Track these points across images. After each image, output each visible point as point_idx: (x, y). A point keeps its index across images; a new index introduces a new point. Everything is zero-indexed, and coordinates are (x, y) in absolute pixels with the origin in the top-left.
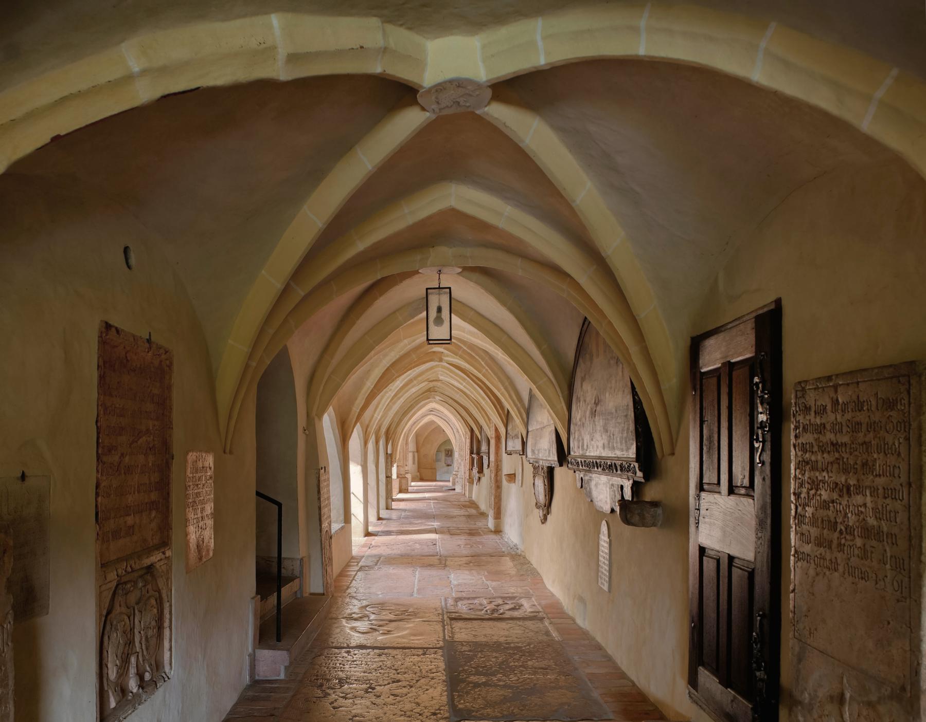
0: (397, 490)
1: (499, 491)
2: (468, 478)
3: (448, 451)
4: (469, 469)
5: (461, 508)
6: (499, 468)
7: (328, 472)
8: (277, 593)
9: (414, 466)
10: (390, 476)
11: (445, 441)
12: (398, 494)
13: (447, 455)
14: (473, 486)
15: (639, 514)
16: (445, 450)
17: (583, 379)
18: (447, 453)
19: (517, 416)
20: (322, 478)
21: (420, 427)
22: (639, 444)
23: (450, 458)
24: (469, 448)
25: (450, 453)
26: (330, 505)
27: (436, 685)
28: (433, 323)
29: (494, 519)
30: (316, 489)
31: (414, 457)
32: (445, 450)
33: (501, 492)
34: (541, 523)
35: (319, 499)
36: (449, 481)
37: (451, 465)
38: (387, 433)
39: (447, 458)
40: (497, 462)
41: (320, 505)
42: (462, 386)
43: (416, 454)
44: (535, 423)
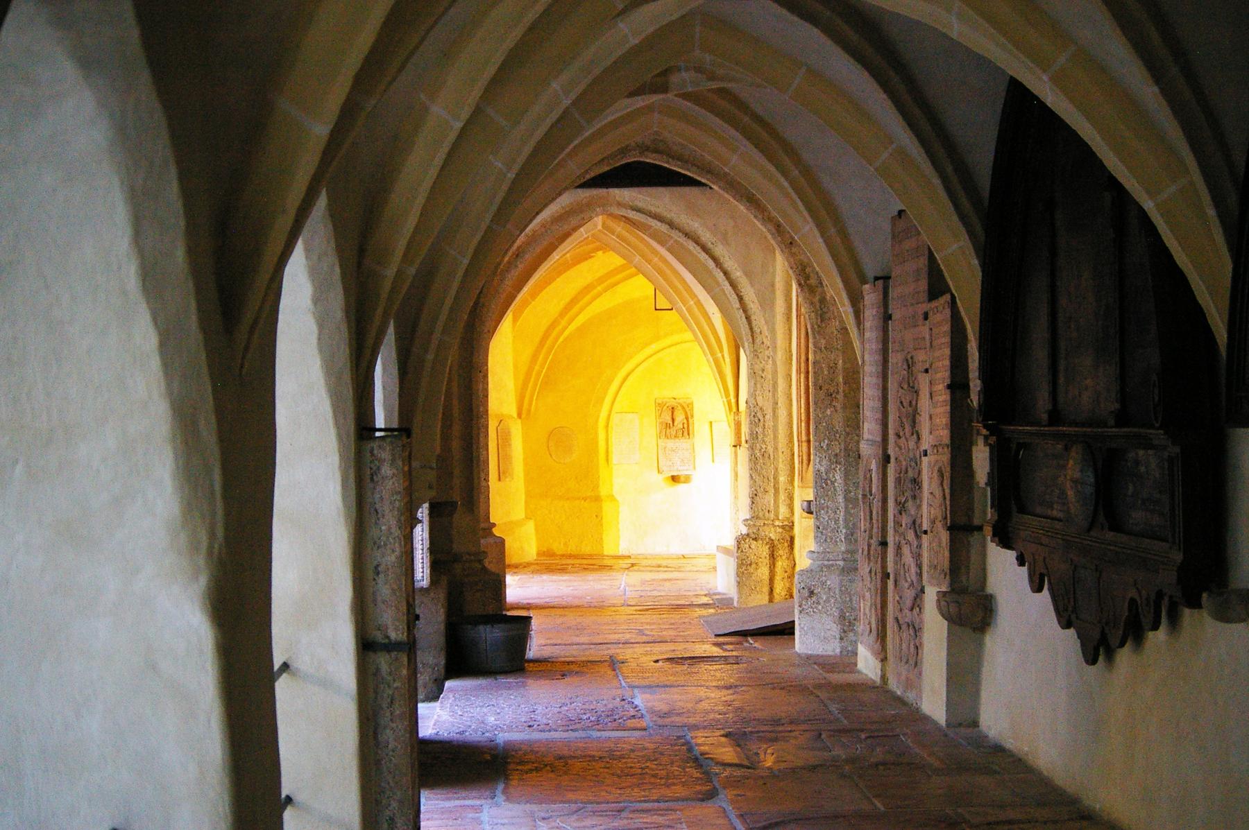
10: (396, 633)
13: (667, 426)
16: (660, 406)
25: (680, 417)
32: (660, 406)
37: (687, 479)
38: (362, 251)
39: (671, 444)
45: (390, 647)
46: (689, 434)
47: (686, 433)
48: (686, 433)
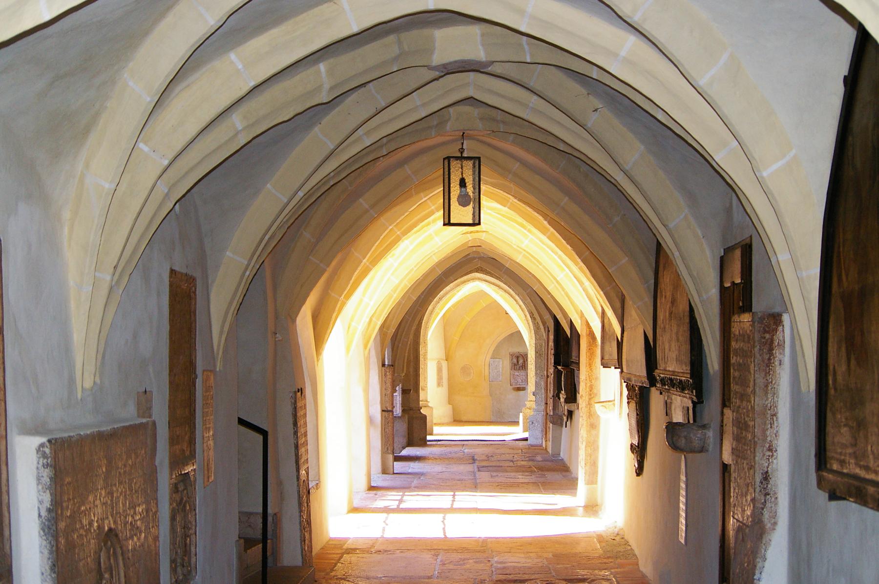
0: (404, 441)
1: (594, 432)
2: (552, 414)
3: (518, 357)
4: (553, 396)
5: (532, 472)
6: (595, 391)
7: (305, 395)
8: (263, 546)
9: (440, 388)
10: (389, 409)
11: (512, 335)
12: (404, 448)
13: (515, 365)
14: (562, 430)
15: (685, 437)
16: (512, 355)
17: (664, 268)
18: (515, 361)
19: (606, 305)
20: (299, 404)
21: (454, 306)
22: (693, 358)
23: (522, 373)
24: (553, 352)
25: (521, 361)
26: (307, 445)
27: (459, 575)
28: (457, 204)
29: (586, 484)
30: (291, 421)
31: (439, 370)
33: (597, 435)
34: (635, 474)
35: (296, 433)
36: (516, 423)
37: (524, 389)
40: (591, 381)
41: (297, 443)
42: (529, 227)
43: (444, 364)
44: (53, 476)
45: (388, 411)
46: (525, 368)
47: (524, 368)
48: (524, 368)
